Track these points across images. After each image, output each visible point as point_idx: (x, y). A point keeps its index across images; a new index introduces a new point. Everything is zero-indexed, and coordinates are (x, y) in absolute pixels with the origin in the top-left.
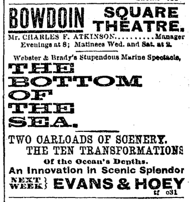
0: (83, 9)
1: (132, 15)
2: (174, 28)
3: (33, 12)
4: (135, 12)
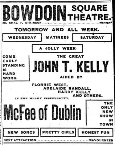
0: (65, 7)
4: (87, 9)
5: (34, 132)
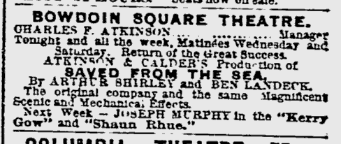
1: (161, 22)
2: (251, 23)
4: (163, 19)
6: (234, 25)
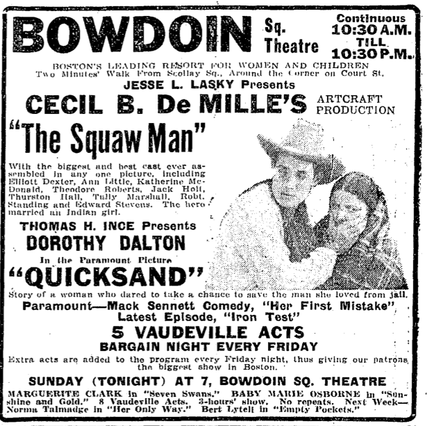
3: (127, 135)
5: (136, 307)
6: (333, 384)
